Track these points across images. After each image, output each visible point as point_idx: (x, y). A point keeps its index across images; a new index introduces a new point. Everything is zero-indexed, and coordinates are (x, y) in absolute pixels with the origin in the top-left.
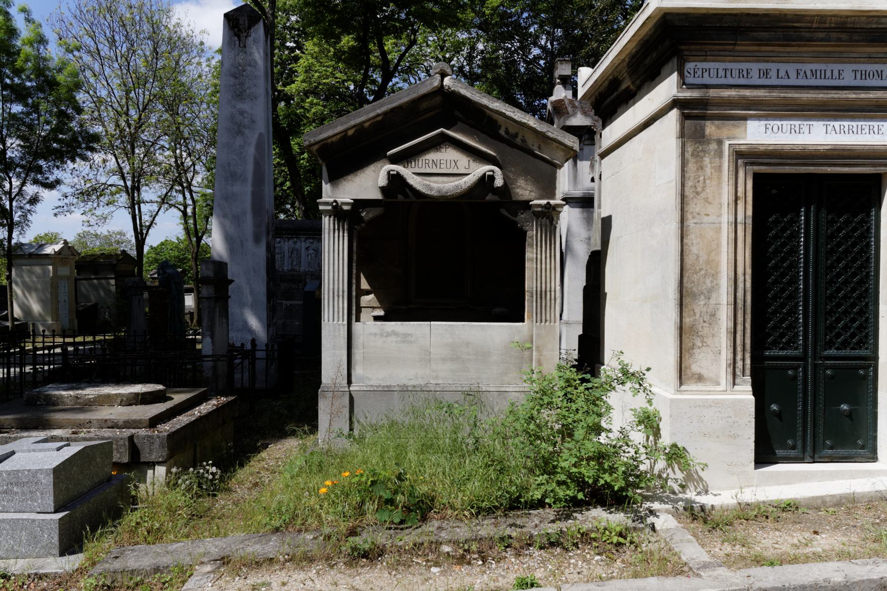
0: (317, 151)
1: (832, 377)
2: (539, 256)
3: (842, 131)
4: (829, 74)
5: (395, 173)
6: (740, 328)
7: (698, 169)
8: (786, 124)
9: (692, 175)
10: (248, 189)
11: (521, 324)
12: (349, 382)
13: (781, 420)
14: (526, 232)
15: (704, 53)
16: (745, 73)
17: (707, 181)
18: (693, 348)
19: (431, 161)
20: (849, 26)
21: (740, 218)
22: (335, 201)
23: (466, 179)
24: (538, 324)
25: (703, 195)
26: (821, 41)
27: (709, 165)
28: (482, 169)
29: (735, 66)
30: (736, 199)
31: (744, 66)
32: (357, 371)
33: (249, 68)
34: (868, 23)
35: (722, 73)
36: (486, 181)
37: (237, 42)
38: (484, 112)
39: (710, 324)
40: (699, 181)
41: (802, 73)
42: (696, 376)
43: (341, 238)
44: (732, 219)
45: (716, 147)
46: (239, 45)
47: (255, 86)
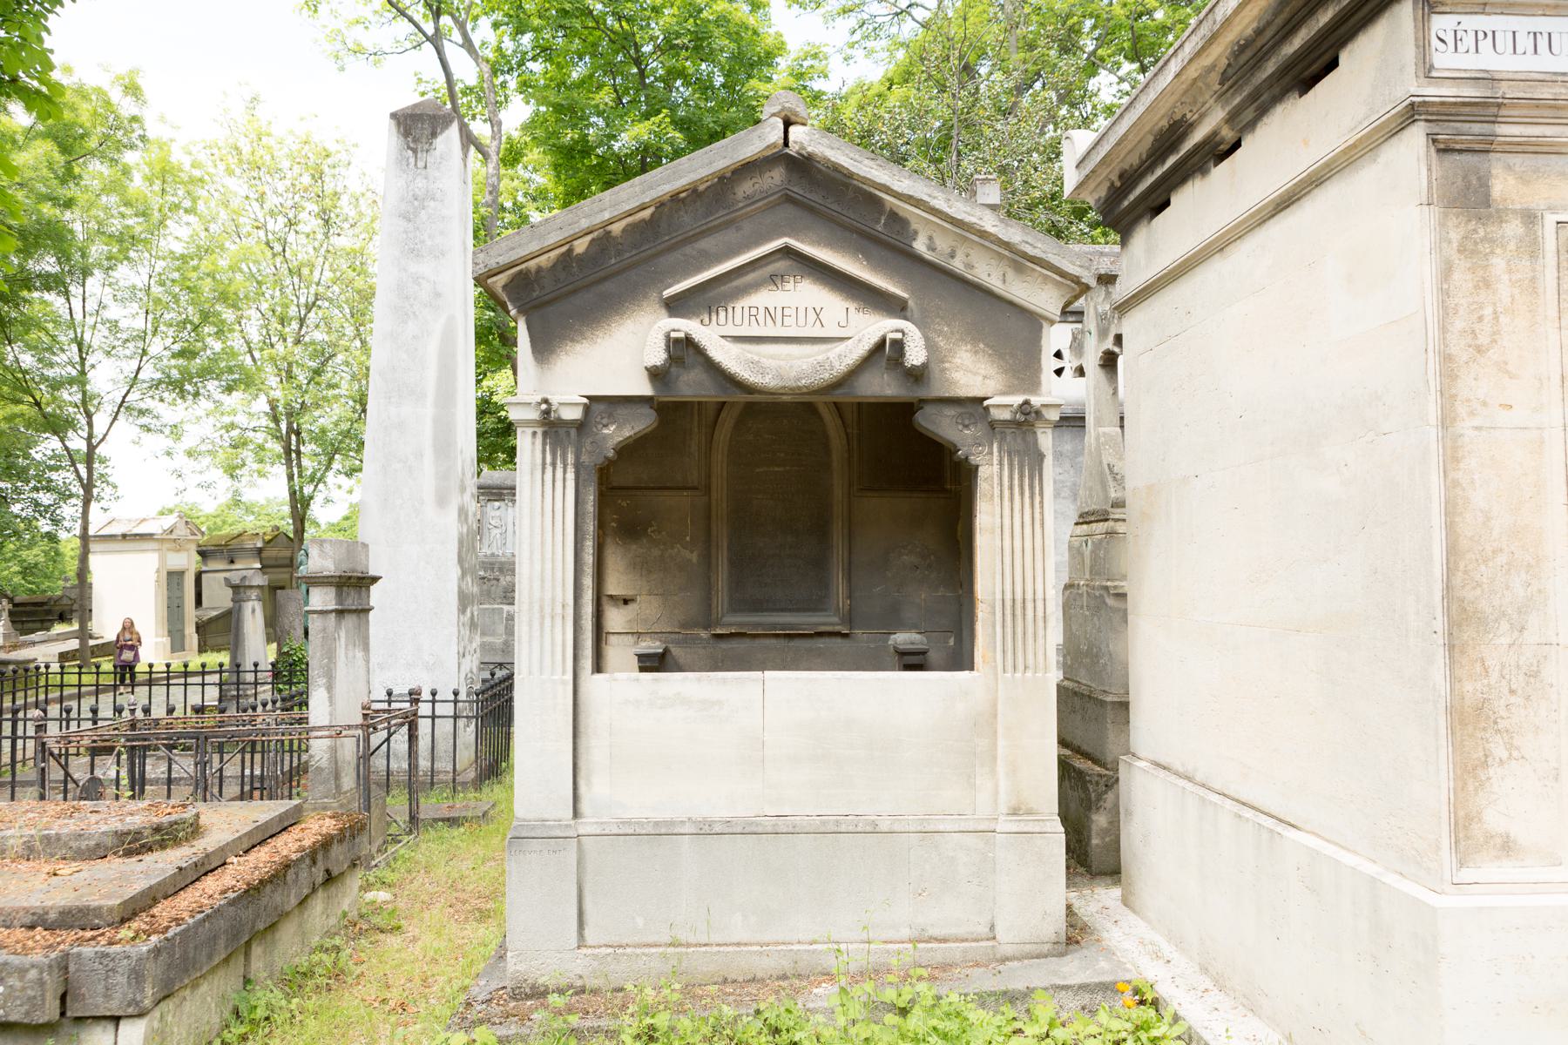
0: (505, 287)
5: (682, 335)
7: (1477, 287)
9: (1463, 301)
10: (428, 411)
14: (977, 467)
17: (1502, 319)
18: (1485, 764)
19: (762, 311)
22: (546, 401)
23: (840, 348)
24: (1008, 675)
27: (1505, 277)
32: (596, 790)
33: (432, 204)
35: (1525, 42)
36: (887, 353)
37: (412, 160)
39: (1528, 698)
40: (1480, 319)
42: (1499, 841)
43: (559, 484)
45: (1521, 230)
46: (416, 165)
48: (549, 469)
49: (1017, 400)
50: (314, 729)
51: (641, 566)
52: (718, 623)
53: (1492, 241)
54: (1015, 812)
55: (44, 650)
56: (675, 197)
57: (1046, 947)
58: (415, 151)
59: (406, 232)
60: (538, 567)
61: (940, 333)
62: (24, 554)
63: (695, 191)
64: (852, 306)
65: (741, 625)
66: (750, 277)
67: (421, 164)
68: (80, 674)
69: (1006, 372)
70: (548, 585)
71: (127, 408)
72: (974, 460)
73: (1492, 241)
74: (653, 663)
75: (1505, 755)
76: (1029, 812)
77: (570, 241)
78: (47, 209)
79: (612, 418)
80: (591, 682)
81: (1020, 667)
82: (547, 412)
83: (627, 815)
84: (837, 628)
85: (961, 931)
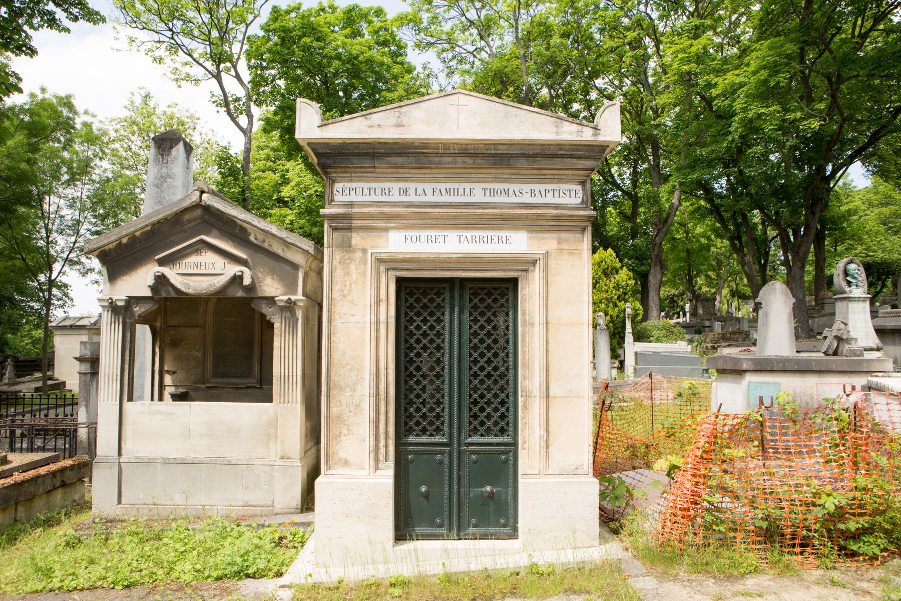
1: (476, 462)
2: (283, 345)
3: (474, 241)
4: (461, 192)
5: (159, 274)
6: (382, 417)
8: (424, 234)
11: (268, 404)
12: (120, 454)
13: (428, 501)
14: (273, 324)
15: (349, 175)
16: (387, 191)
17: (353, 286)
18: (339, 435)
20: (470, 151)
21: (383, 318)
22: (111, 299)
23: (220, 278)
25: (349, 298)
26: (448, 164)
28: (234, 269)
29: (378, 186)
30: (378, 302)
31: (386, 185)
33: (169, 180)
34: (487, 149)
35: (366, 191)
36: (237, 279)
37: (161, 160)
38: (235, 222)
39: (356, 414)
40: (345, 286)
41: (437, 191)
42: (343, 461)
43: (117, 330)
44: (374, 319)
45: (361, 255)
47: (173, 194)
48: (113, 324)
49: (286, 298)
50: (80, 423)
51: (178, 359)
52: (207, 382)
53: (350, 259)
54: (282, 458)
55: (27, 387)
56: (159, 222)
57: (293, 510)
58: (162, 155)
59: (157, 193)
60: (108, 361)
61: (260, 272)
62: (34, 333)
63: (166, 219)
64: (226, 262)
65: (216, 383)
66: (189, 251)
67: (165, 161)
68: (40, 399)
69: (284, 286)
70: (111, 367)
71: (70, 261)
72: (272, 321)
73: (350, 259)
74: (176, 397)
75: (347, 433)
76: (288, 458)
77: (120, 239)
78: (23, 166)
79: (137, 304)
80: (127, 405)
81: (286, 401)
82: (112, 303)
83: (139, 455)
84: (255, 385)
85: (262, 503)
